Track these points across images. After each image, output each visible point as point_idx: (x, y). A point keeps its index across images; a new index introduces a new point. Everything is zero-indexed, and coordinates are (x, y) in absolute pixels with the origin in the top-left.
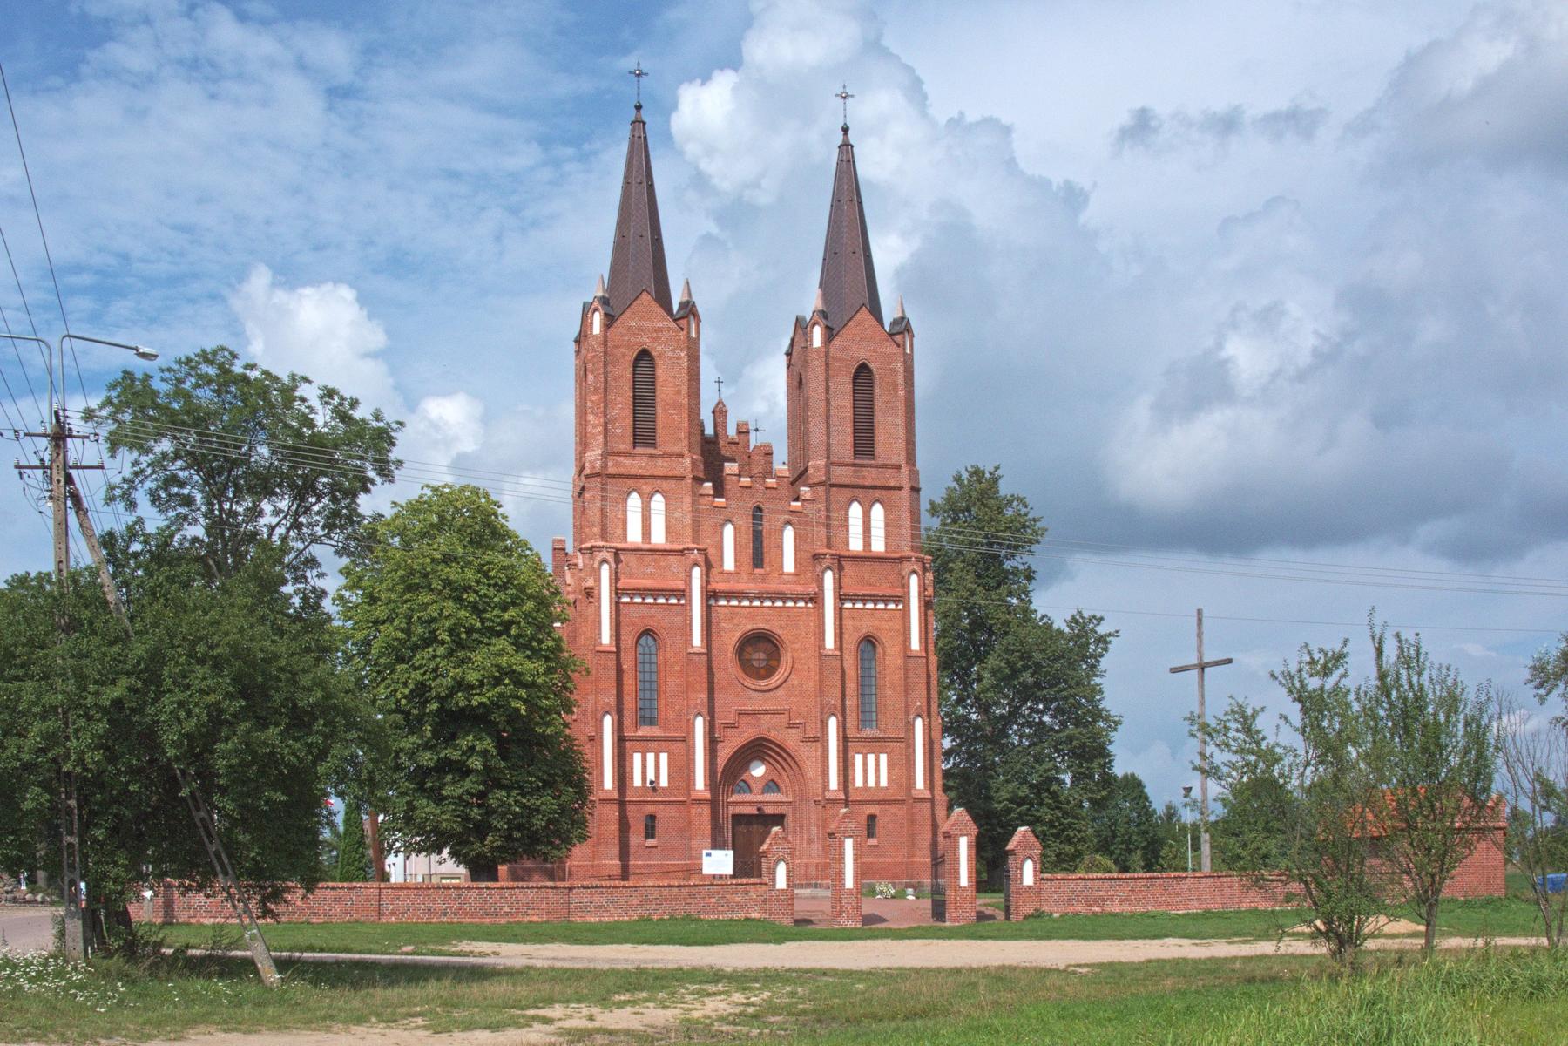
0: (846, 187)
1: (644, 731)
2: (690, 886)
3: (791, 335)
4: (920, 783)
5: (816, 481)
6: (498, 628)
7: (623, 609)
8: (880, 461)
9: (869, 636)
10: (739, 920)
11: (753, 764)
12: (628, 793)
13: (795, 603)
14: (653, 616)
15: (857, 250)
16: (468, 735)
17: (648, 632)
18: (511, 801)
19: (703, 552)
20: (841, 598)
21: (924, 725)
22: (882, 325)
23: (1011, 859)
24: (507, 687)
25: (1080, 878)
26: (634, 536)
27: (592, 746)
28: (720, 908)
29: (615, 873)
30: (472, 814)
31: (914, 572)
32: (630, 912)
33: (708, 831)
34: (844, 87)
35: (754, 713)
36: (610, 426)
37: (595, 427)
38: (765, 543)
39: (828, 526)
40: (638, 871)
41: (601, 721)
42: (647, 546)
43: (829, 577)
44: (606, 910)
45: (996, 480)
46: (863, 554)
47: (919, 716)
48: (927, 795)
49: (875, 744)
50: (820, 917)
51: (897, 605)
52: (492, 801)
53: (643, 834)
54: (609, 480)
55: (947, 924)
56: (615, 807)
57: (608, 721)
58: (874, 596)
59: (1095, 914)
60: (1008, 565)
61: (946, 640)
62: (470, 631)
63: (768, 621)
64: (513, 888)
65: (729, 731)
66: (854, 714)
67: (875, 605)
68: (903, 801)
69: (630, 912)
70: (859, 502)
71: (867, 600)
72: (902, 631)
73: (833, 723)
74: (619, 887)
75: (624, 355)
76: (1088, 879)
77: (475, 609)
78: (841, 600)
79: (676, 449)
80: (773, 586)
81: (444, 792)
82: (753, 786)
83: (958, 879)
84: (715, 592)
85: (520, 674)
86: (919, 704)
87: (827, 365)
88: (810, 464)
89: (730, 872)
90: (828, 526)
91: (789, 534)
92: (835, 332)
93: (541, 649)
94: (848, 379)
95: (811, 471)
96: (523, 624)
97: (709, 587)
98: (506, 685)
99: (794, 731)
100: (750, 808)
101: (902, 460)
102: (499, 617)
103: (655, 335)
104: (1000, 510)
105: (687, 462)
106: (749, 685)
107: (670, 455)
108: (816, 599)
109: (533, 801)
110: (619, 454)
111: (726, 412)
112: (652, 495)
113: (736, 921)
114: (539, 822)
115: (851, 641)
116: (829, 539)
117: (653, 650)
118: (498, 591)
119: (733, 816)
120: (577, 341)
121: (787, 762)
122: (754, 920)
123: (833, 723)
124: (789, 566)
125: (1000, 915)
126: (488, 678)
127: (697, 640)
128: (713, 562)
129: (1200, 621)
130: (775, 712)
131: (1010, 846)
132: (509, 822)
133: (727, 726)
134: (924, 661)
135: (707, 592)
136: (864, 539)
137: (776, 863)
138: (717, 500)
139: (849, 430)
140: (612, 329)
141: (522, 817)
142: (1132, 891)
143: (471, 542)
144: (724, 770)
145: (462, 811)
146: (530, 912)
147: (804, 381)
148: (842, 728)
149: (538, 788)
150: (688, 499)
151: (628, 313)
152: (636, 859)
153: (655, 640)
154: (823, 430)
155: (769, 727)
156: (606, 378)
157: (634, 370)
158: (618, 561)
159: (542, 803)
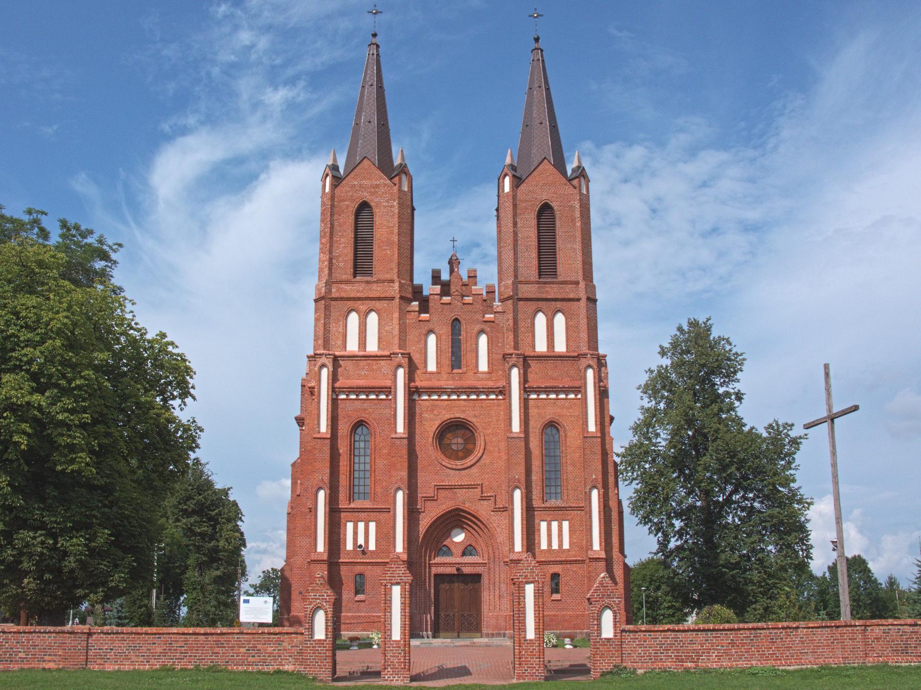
4: (596, 546)
7: (341, 405)
8: (560, 279)
9: (552, 421)
12: (342, 555)
13: (487, 396)
14: (365, 410)
15: (544, 121)
20: (526, 389)
25: (669, 630)
26: (352, 346)
28: (250, 659)
31: (589, 366)
32: (153, 661)
35: (451, 488)
36: (334, 261)
38: (463, 347)
47: (595, 487)
49: (559, 513)
51: (576, 395)
53: (353, 590)
58: (555, 388)
59: (687, 670)
63: (464, 411)
64: (30, 633)
65: (429, 504)
66: (539, 488)
67: (557, 395)
68: (583, 561)
69: (153, 661)
70: (543, 313)
74: (142, 634)
76: (679, 631)
79: (388, 276)
84: (417, 388)
86: (594, 477)
89: (269, 619)
91: (483, 340)
94: (533, 215)
99: (486, 502)
103: (373, 190)
105: (396, 286)
107: (383, 281)
108: (504, 391)
110: (341, 282)
115: (536, 425)
122: (286, 672)
123: (517, 494)
124: (483, 366)
127: (400, 428)
129: (827, 375)
138: (422, 315)
139: (534, 255)
142: (732, 643)
144: (425, 536)
146: (46, 658)
150: (396, 315)
152: (349, 611)
154: (511, 253)
155: (465, 500)
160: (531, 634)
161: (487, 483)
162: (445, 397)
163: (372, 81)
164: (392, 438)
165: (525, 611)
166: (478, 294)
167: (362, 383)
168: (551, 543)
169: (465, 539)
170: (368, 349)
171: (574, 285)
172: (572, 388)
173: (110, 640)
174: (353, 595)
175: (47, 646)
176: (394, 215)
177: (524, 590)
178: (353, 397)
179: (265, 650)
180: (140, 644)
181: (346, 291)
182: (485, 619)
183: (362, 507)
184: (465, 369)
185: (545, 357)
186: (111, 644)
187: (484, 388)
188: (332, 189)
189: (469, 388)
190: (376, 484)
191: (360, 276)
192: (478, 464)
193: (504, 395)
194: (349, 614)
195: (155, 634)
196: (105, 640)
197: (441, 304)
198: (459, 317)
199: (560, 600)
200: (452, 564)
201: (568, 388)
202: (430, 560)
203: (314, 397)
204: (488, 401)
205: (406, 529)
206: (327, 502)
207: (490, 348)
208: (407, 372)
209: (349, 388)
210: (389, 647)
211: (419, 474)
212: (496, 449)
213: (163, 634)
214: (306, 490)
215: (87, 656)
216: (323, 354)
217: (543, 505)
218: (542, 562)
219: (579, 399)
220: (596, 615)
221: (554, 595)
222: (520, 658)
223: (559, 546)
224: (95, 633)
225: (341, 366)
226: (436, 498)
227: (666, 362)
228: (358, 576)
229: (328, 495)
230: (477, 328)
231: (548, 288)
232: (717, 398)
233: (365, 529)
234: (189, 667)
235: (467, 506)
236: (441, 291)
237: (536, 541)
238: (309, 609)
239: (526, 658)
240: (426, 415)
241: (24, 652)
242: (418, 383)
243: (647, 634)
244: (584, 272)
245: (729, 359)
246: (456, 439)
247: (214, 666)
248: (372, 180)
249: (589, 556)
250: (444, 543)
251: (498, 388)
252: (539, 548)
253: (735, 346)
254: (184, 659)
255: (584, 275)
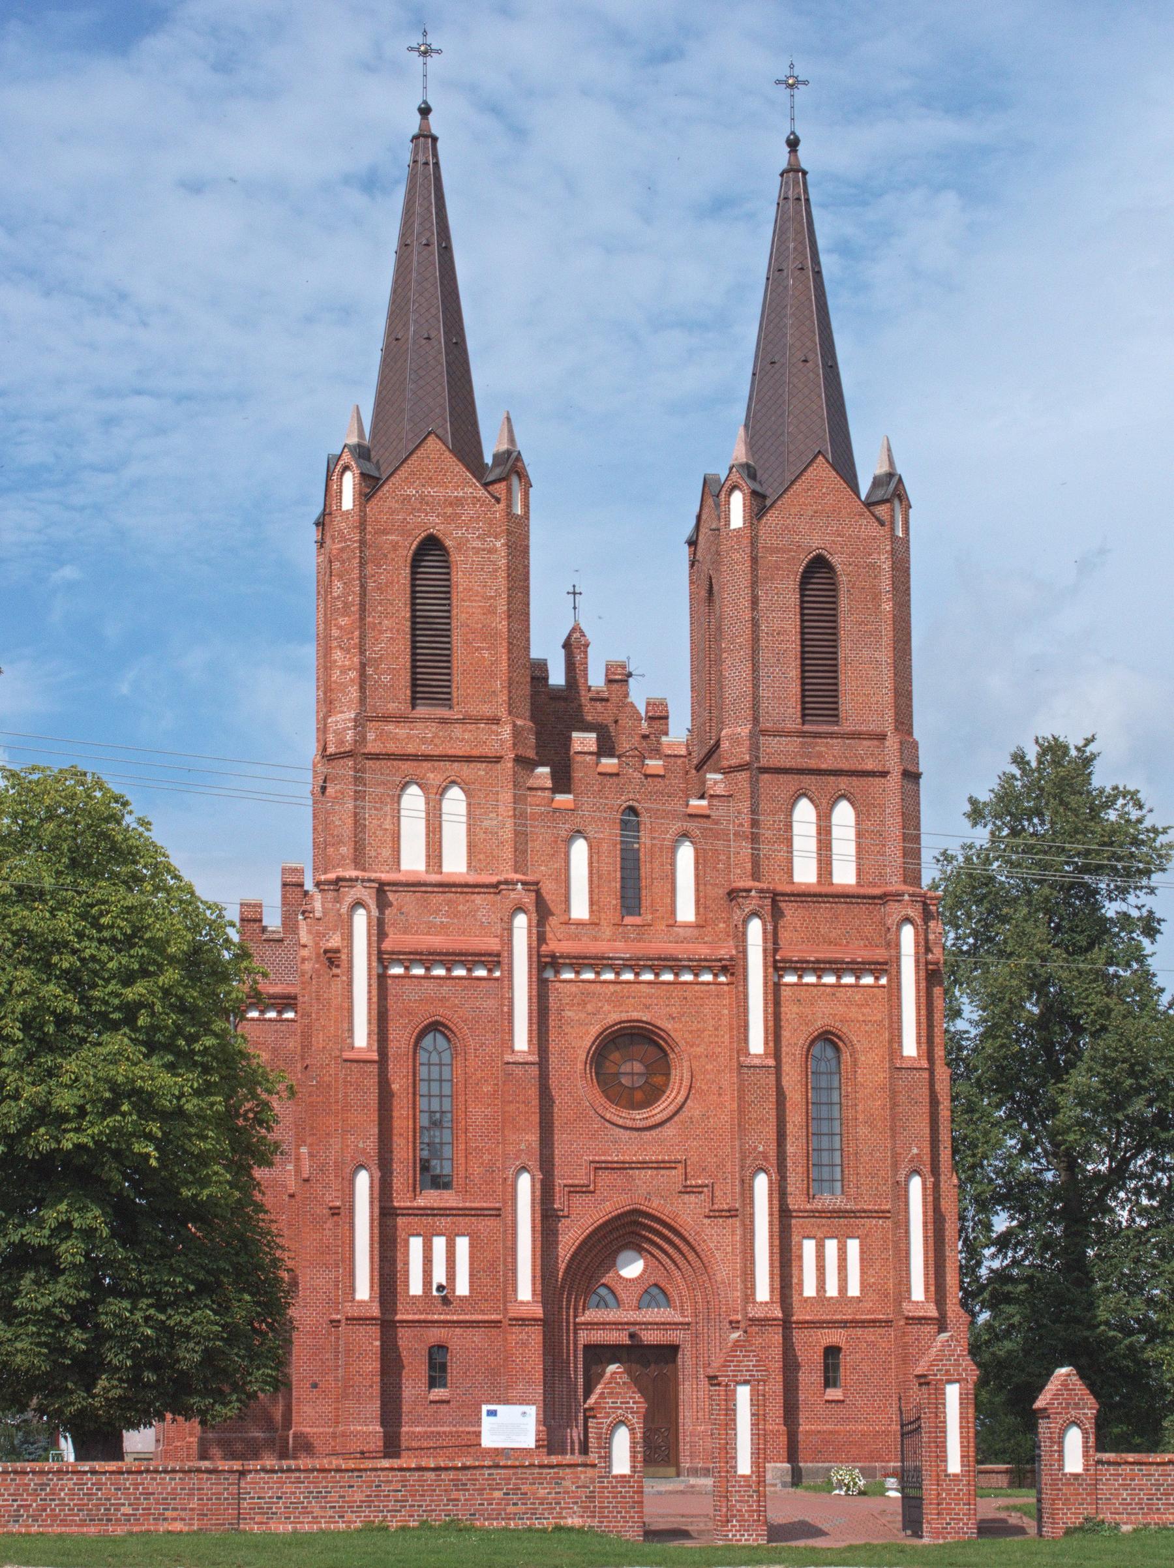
0: (792, 245)
1: (430, 1198)
2: (456, 1469)
3: (697, 509)
4: (918, 1292)
5: (733, 762)
6: (116, 1016)
7: (393, 988)
8: (847, 727)
10: (544, 1531)
11: (623, 1256)
12: (400, 1306)
13: (696, 975)
14: (443, 1000)
15: (811, 357)
16: (61, 1202)
17: (435, 1027)
18: (138, 1316)
19: (534, 887)
20: (776, 966)
21: (924, 1188)
22: (855, 489)
23: (1042, 1424)
24: (127, 1116)
26: (413, 860)
27: (337, 1225)
29: (372, 1447)
30: (71, 1341)
31: (907, 920)
33: (538, 1375)
34: (792, 66)
36: (370, 671)
37: (344, 672)
38: (645, 870)
39: (755, 838)
40: (414, 1444)
41: (352, 1183)
42: (434, 878)
43: (755, 928)
44: (306, 1512)
45: (1088, 761)
46: (818, 890)
47: (917, 1172)
48: (933, 1312)
50: (702, 1526)
51: (877, 978)
52: (103, 1318)
54: (369, 763)
55: (926, 1540)
56: (375, 1331)
57: (363, 1181)
58: (835, 962)
60: (1111, 909)
61: (999, 1041)
62: (63, 1020)
63: (647, 1007)
65: (577, 1199)
66: (800, 1170)
67: (839, 977)
68: (888, 1323)
69: (349, 1516)
71: (824, 970)
72: (886, 1023)
73: (761, 1184)
75: (395, 546)
77: (72, 980)
78: (776, 969)
79: (486, 710)
80: (659, 945)
81: (16, 1303)
82: (623, 1295)
83: (945, 1460)
84: (553, 956)
85: (151, 1095)
86: (915, 1151)
87: (754, 560)
88: (724, 733)
90: (755, 838)
91: (686, 855)
92: (768, 503)
93: (192, 1052)
95: (725, 745)
96: (158, 1008)
97: (544, 948)
98: (123, 1115)
99: (693, 1198)
100: (615, 1334)
101: (887, 724)
102: (118, 995)
103: (449, 510)
104: (1095, 813)
105: (506, 732)
106: (615, 1119)
107: (477, 720)
108: (734, 968)
109: (177, 1318)
110: (386, 718)
111: (587, 645)
112: (445, 789)
113: (538, 1530)
114: (189, 1355)
115: (794, 1040)
116: (756, 862)
117: (446, 1057)
118: (119, 951)
119: (585, 1346)
120: (320, 524)
121: (683, 1255)
122: (571, 1529)
123: (761, 1184)
124: (686, 911)
125: (1030, 1524)
126: (93, 1102)
127: (521, 1041)
128: (551, 906)
130: (660, 1166)
131: (1039, 1404)
132: (133, 1357)
133: (575, 1190)
134: (926, 1075)
135: (539, 956)
136: (819, 861)
137: (613, 1428)
139: (794, 673)
140: (374, 501)
141: (159, 1346)
143: (74, 864)
144: (568, 1267)
145: (52, 1335)
146: (168, 1514)
147: (715, 588)
148: (779, 1193)
149: (189, 1295)
150: (506, 796)
151: (402, 473)
153: (448, 1040)
154: (746, 669)
156: (363, 587)
157: (413, 573)
158: (383, 904)
159: (194, 1322)
160: (744, 1466)
161: (695, 1159)
162: (609, 976)
163: (428, 234)
164: (508, 1063)
165: (945, 1427)
166: (675, 756)
167: (436, 942)
168: (824, 1284)
169: (644, 1271)
170: (445, 869)
171: (876, 742)
172: (870, 963)
173: (276, 1483)
174: (425, 1388)
175: (168, 1494)
176: (496, 571)
177: (944, 1394)
178: (419, 971)
179: (534, 1494)
180: (326, 1487)
181: (395, 739)
182: (688, 1439)
183: (442, 1205)
184: (649, 917)
185: (815, 895)
186: (278, 1488)
187: (690, 960)
188: (361, 504)
189: (659, 959)
190: (470, 1157)
191: (424, 705)
192: (676, 1119)
193: (732, 974)
194: (418, 1429)
195: (353, 1470)
196: (268, 1483)
197: (600, 774)
198: (635, 804)
199: (843, 1401)
200: (621, 1324)
201: (863, 963)
202: (576, 1316)
203: (336, 971)
204: (697, 987)
205: (539, 1254)
206: (376, 1195)
207: (701, 873)
208: (534, 922)
209: (410, 953)
210: (734, 1486)
211: (556, 1137)
212: (714, 1087)
213: (365, 1470)
214: (322, 1168)
215: (239, 1509)
216: (357, 879)
217: (808, 1207)
218: (807, 1322)
219: (883, 986)
220: (1056, 1435)
221: (828, 1390)
222: (938, 1504)
223: (818, 1291)
224: (250, 1471)
225: (391, 905)
226: (591, 1188)
227: (981, 836)
228: (435, 1349)
229: (376, 1182)
230: (676, 826)
231: (821, 746)
232: (1101, 929)
233: (448, 1251)
234: (411, 1524)
235: (654, 1205)
236: (599, 747)
237: (795, 1280)
238: (605, 1426)
239: (948, 1504)
240: (569, 1014)
241: (130, 1505)
242: (554, 946)
243: (1136, 1468)
244: (896, 714)
245: (1136, 842)
246: (629, 1064)
247: (452, 1521)
248: (447, 487)
249: (906, 1313)
250: (603, 1281)
251: (720, 960)
252: (801, 1294)
253: (1151, 811)
254: (400, 1511)
255: (896, 721)
